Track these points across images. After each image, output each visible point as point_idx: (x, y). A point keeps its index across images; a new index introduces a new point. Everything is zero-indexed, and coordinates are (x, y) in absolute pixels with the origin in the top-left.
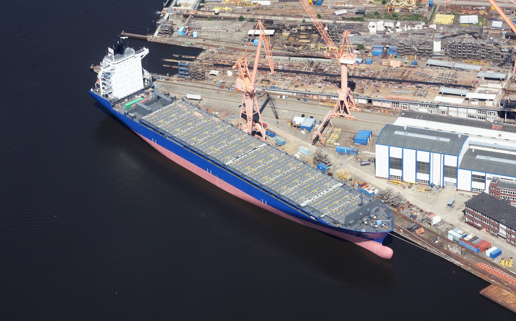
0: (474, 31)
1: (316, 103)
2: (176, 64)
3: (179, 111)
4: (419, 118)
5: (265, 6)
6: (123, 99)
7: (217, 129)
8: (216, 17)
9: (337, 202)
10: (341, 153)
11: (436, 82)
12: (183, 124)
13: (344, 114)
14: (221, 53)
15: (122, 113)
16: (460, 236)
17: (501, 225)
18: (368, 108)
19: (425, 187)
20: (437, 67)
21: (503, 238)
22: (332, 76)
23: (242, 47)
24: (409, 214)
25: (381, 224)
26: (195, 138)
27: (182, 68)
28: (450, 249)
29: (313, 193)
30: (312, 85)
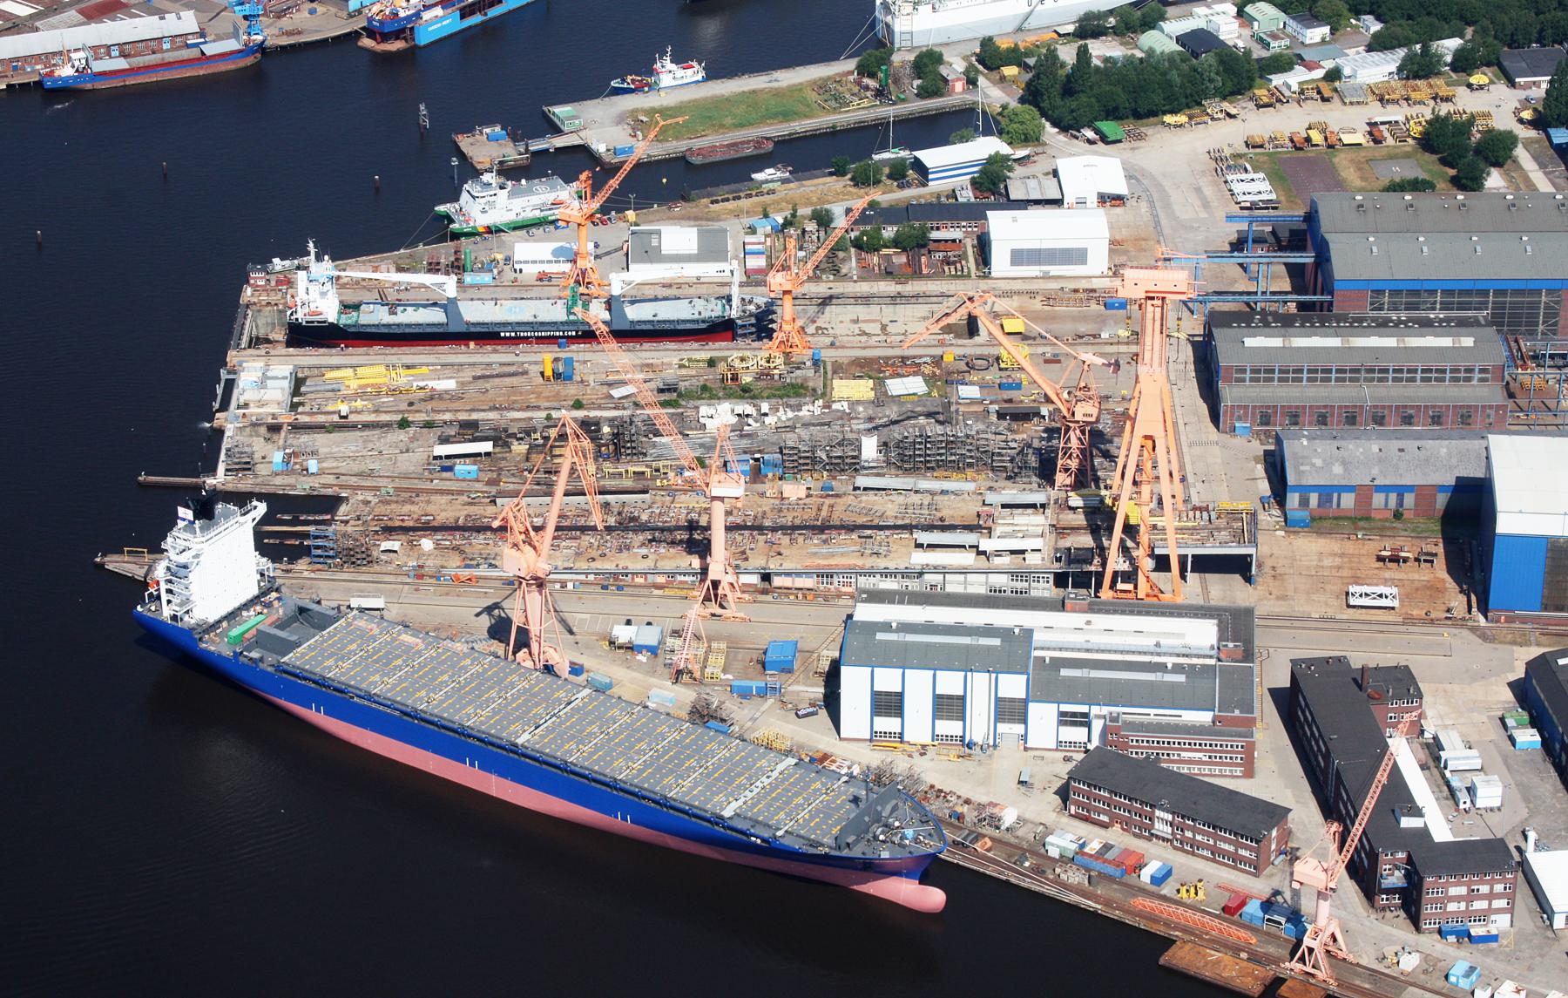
0: (933, 409)
1: (645, 591)
2: (306, 535)
3: (361, 637)
4: (901, 602)
5: (446, 392)
6: (219, 622)
7: (465, 669)
8: (344, 425)
9: (800, 800)
10: (745, 694)
11: (900, 522)
12: (385, 662)
13: (719, 611)
14: (388, 503)
15: (228, 653)
16: (1074, 847)
17: (1158, 813)
18: (764, 592)
19: (953, 752)
20: (897, 494)
21: (1164, 839)
22: (662, 530)
23: (428, 485)
24: (947, 812)
25: (913, 837)
26: (423, 693)
27: (319, 542)
28: (1064, 877)
29: (739, 787)
30: (625, 554)
